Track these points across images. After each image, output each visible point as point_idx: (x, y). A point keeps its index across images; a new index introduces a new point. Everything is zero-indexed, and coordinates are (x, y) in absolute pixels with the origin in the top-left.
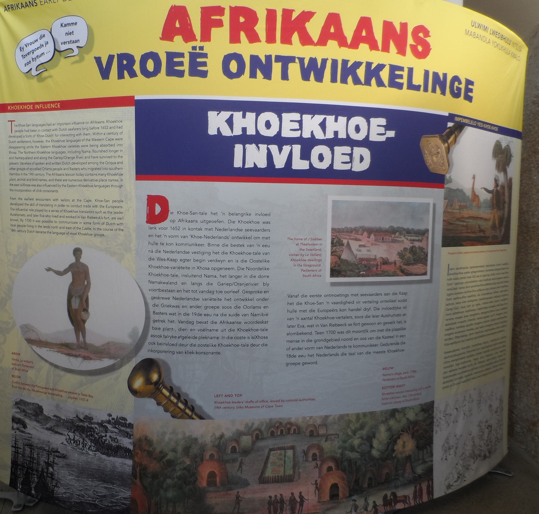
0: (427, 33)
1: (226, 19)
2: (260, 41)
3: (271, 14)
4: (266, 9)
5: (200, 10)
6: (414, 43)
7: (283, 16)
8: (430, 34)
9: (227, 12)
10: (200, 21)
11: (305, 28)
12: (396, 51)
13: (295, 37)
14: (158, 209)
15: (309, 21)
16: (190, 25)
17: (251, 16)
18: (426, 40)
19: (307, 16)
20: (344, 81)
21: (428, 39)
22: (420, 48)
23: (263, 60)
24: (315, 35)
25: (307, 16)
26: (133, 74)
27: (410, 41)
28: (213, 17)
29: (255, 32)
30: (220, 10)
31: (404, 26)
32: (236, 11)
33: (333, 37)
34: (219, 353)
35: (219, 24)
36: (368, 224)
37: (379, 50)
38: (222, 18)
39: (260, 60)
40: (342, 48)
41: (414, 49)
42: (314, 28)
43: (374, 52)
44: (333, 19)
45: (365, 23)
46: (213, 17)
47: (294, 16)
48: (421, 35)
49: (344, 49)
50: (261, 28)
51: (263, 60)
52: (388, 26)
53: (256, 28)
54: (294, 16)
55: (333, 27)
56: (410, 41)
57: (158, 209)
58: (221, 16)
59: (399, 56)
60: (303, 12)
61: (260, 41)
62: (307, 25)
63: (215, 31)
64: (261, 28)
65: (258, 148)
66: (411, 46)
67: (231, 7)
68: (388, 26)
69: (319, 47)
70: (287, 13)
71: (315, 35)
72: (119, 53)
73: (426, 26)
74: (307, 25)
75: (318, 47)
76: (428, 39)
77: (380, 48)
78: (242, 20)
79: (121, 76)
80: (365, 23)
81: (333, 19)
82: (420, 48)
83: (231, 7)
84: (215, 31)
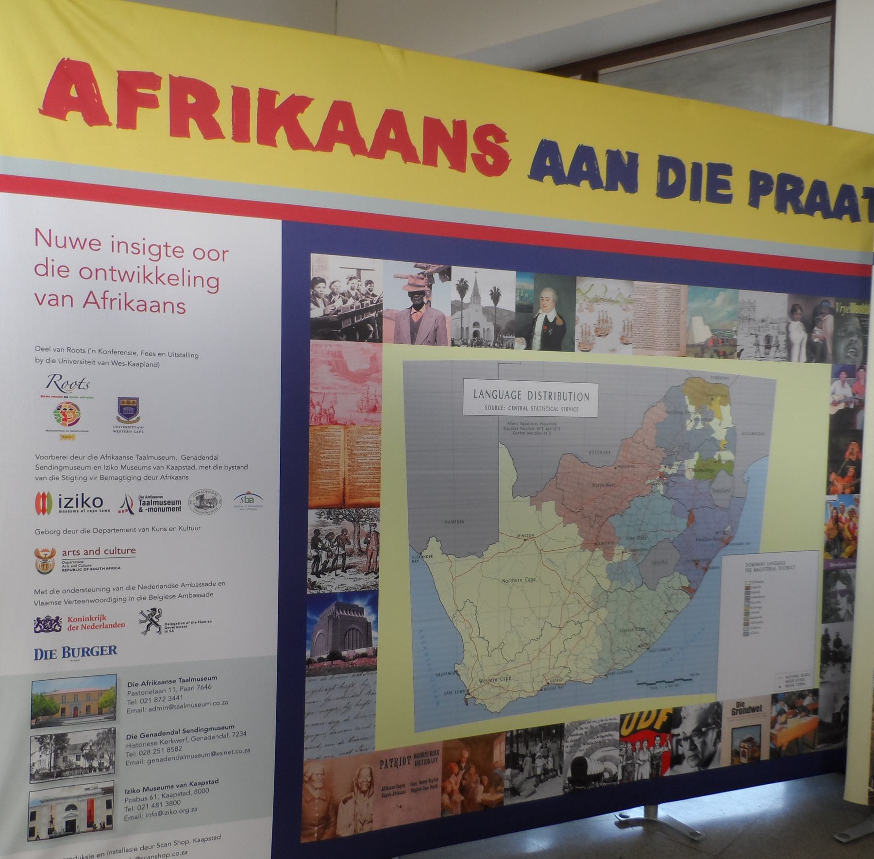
0: (501, 136)
1: (163, 95)
2: (223, 137)
3: (240, 96)
4: (232, 87)
6: (478, 152)
7: (260, 99)
8: (507, 137)
9: (165, 84)
10: (116, 93)
11: (297, 123)
13: (281, 135)
14: (672, 178)
15: (302, 112)
16: (98, 96)
17: (207, 96)
19: (299, 103)
20: (267, 138)
21: (503, 145)
22: (490, 160)
24: (313, 133)
25: (299, 103)
26: (211, 131)
27: (472, 148)
28: (140, 90)
29: (214, 121)
30: (153, 80)
31: (460, 126)
34: (211, 595)
35: (152, 102)
36: (375, 779)
37: (418, 162)
38: (157, 93)
41: (479, 161)
42: (311, 122)
43: (410, 164)
44: (341, 111)
46: (140, 90)
47: (279, 101)
48: (491, 139)
50: (224, 116)
52: (432, 127)
53: (216, 116)
54: (279, 101)
55: (341, 125)
56: (472, 148)
57: (672, 178)
58: (154, 89)
59: (454, 171)
60: (293, 97)
61: (223, 137)
62: (300, 117)
63: (142, 113)
64: (224, 116)
65: (713, 568)
66: (474, 156)
67: (171, 77)
68: (432, 127)
69: (320, 154)
70: (267, 96)
71: (313, 133)
73: (500, 125)
74: (300, 117)
76: (503, 145)
77: (604, 185)
78: (191, 100)
79: (179, 129)
81: (341, 111)
82: (490, 160)
83: (171, 77)
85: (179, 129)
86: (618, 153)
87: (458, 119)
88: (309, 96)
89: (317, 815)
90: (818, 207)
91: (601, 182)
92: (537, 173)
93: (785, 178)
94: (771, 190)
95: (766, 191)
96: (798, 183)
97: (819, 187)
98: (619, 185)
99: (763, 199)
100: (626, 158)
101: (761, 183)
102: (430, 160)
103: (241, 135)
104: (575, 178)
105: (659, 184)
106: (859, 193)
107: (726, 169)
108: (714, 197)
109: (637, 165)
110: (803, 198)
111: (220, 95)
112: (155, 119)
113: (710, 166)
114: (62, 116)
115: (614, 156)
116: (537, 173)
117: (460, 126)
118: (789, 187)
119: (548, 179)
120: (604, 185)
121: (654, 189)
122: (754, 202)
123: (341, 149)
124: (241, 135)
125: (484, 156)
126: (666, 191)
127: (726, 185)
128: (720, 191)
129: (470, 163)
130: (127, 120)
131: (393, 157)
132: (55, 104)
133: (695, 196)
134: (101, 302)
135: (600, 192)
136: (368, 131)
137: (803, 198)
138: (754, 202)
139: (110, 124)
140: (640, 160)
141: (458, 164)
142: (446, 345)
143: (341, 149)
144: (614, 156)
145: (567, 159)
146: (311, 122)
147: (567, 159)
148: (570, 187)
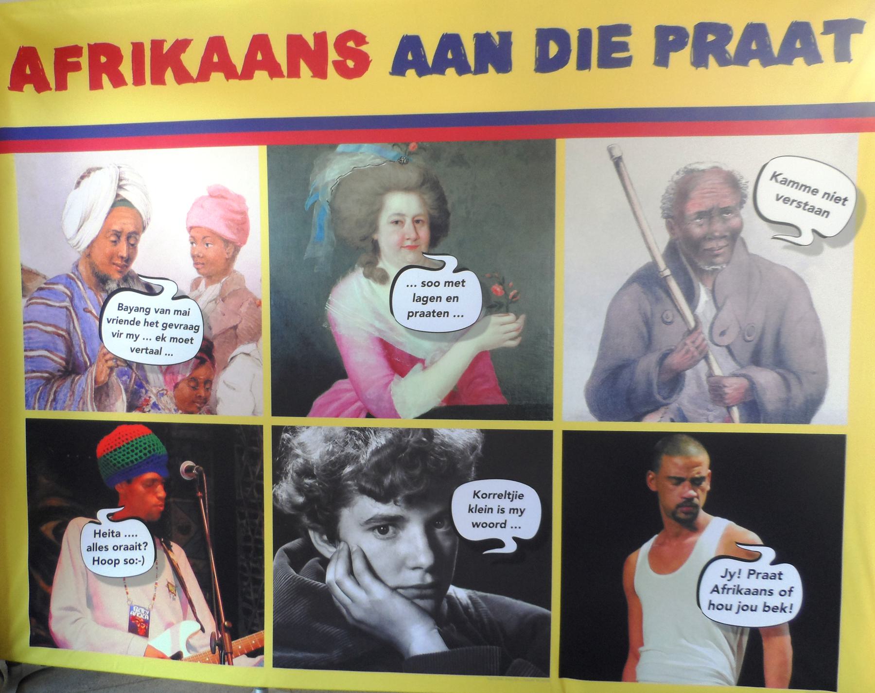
0: (360, 39)
1: (84, 61)
3: (138, 48)
5: (54, 52)
7: (152, 49)
8: (367, 39)
12: (311, 74)
13: (169, 75)
14: (553, 49)
16: (43, 70)
17: (113, 53)
18: (361, 52)
19: (182, 45)
20: (158, 79)
21: (364, 48)
22: (350, 64)
23: (311, 43)
25: (182, 45)
26: (118, 81)
27: (333, 55)
28: (70, 60)
30: (76, 51)
31: (320, 38)
32: (96, 50)
33: (217, 68)
35: (77, 67)
39: (304, 43)
40: (231, 81)
42: (192, 60)
43: (276, 80)
44: (217, 45)
45: (260, 43)
46: (70, 60)
47: (166, 47)
48: (351, 44)
49: (234, 82)
50: (126, 69)
51: (311, 43)
52: (295, 43)
54: (166, 47)
55: (216, 53)
56: (333, 55)
57: (553, 49)
62: (183, 57)
64: (126, 69)
66: (335, 63)
67: (89, 45)
69: (200, 85)
70: (157, 45)
72: (92, 43)
74: (183, 57)
75: (199, 84)
76: (364, 48)
77: (473, 69)
78: (103, 59)
80: (260, 43)
81: (217, 45)
82: (350, 64)
83: (89, 45)
84: (71, 77)
85: (95, 84)
86: (488, 35)
87: (319, 31)
88: (189, 38)
89: (651, 476)
90: (753, 55)
91: (469, 67)
92: (399, 68)
93: (703, 29)
94: (685, 44)
95: (679, 45)
96: (723, 31)
97: (756, 32)
98: (490, 67)
99: (673, 56)
100: (497, 39)
101: (671, 38)
102: (294, 72)
103: (139, 80)
104: (439, 67)
105: (537, 60)
106: (817, 28)
107: (625, 30)
108: (606, 62)
109: (510, 44)
110: (731, 48)
111: (123, 52)
112: (79, 80)
113: (603, 30)
114: (20, 89)
115: (482, 40)
116: (399, 68)
117: (320, 38)
118: (711, 38)
119: (411, 73)
120: (473, 69)
121: (532, 64)
122: (662, 60)
123: (217, 77)
124: (139, 80)
125: (345, 61)
126: (545, 64)
127: (624, 47)
128: (615, 55)
129: (331, 69)
130: (62, 85)
131: (261, 76)
132: (17, 82)
133: (584, 64)
134: (721, 590)
135: (468, 77)
136: (238, 58)
137: (731, 48)
138: (662, 60)
139: (51, 89)
140: (514, 39)
141: (320, 72)
142: (544, 672)
143: (217, 77)
144: (482, 40)
145: (430, 51)
146: (192, 60)
147: (430, 51)
148: (435, 77)
